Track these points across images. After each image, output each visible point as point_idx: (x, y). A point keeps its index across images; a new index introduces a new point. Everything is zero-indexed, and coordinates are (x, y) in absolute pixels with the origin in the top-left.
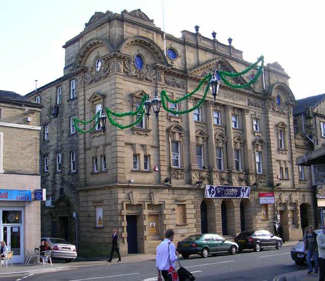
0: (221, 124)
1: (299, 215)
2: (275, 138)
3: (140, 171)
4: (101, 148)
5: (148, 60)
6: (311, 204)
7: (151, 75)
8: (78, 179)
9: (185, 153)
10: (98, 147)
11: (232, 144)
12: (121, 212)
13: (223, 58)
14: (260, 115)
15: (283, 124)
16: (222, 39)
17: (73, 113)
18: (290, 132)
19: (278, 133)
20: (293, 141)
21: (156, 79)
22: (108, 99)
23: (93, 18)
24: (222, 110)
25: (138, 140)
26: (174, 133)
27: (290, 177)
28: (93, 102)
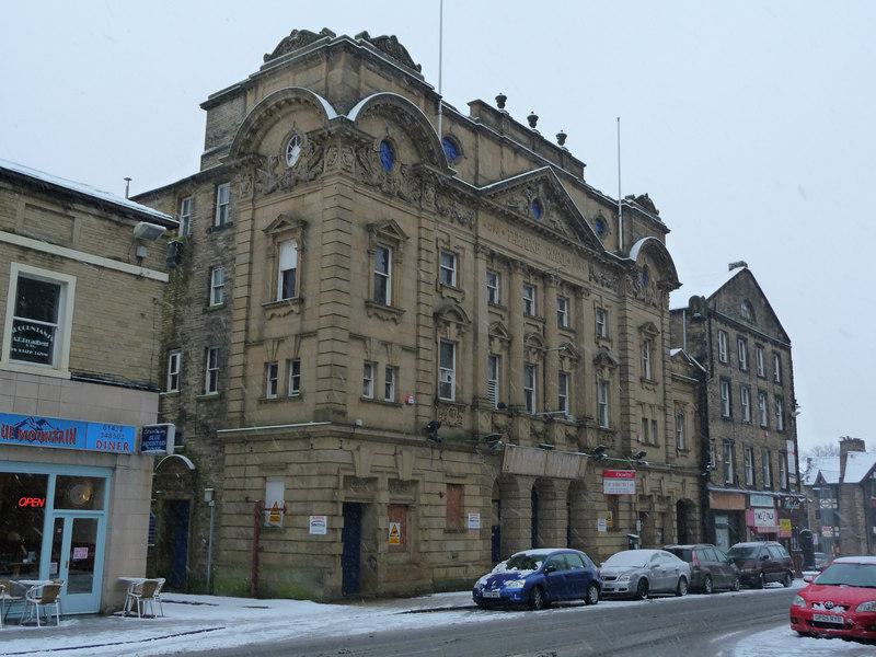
3: (375, 402)
4: (291, 343)
5: (406, 155)
6: (696, 502)
8: (222, 412)
9: (469, 370)
10: (280, 341)
13: (551, 169)
16: (548, 132)
17: (218, 258)
22: (314, 232)
23: (285, 45)
24: (539, 284)
26: (447, 323)
27: (661, 441)
28: (275, 236)
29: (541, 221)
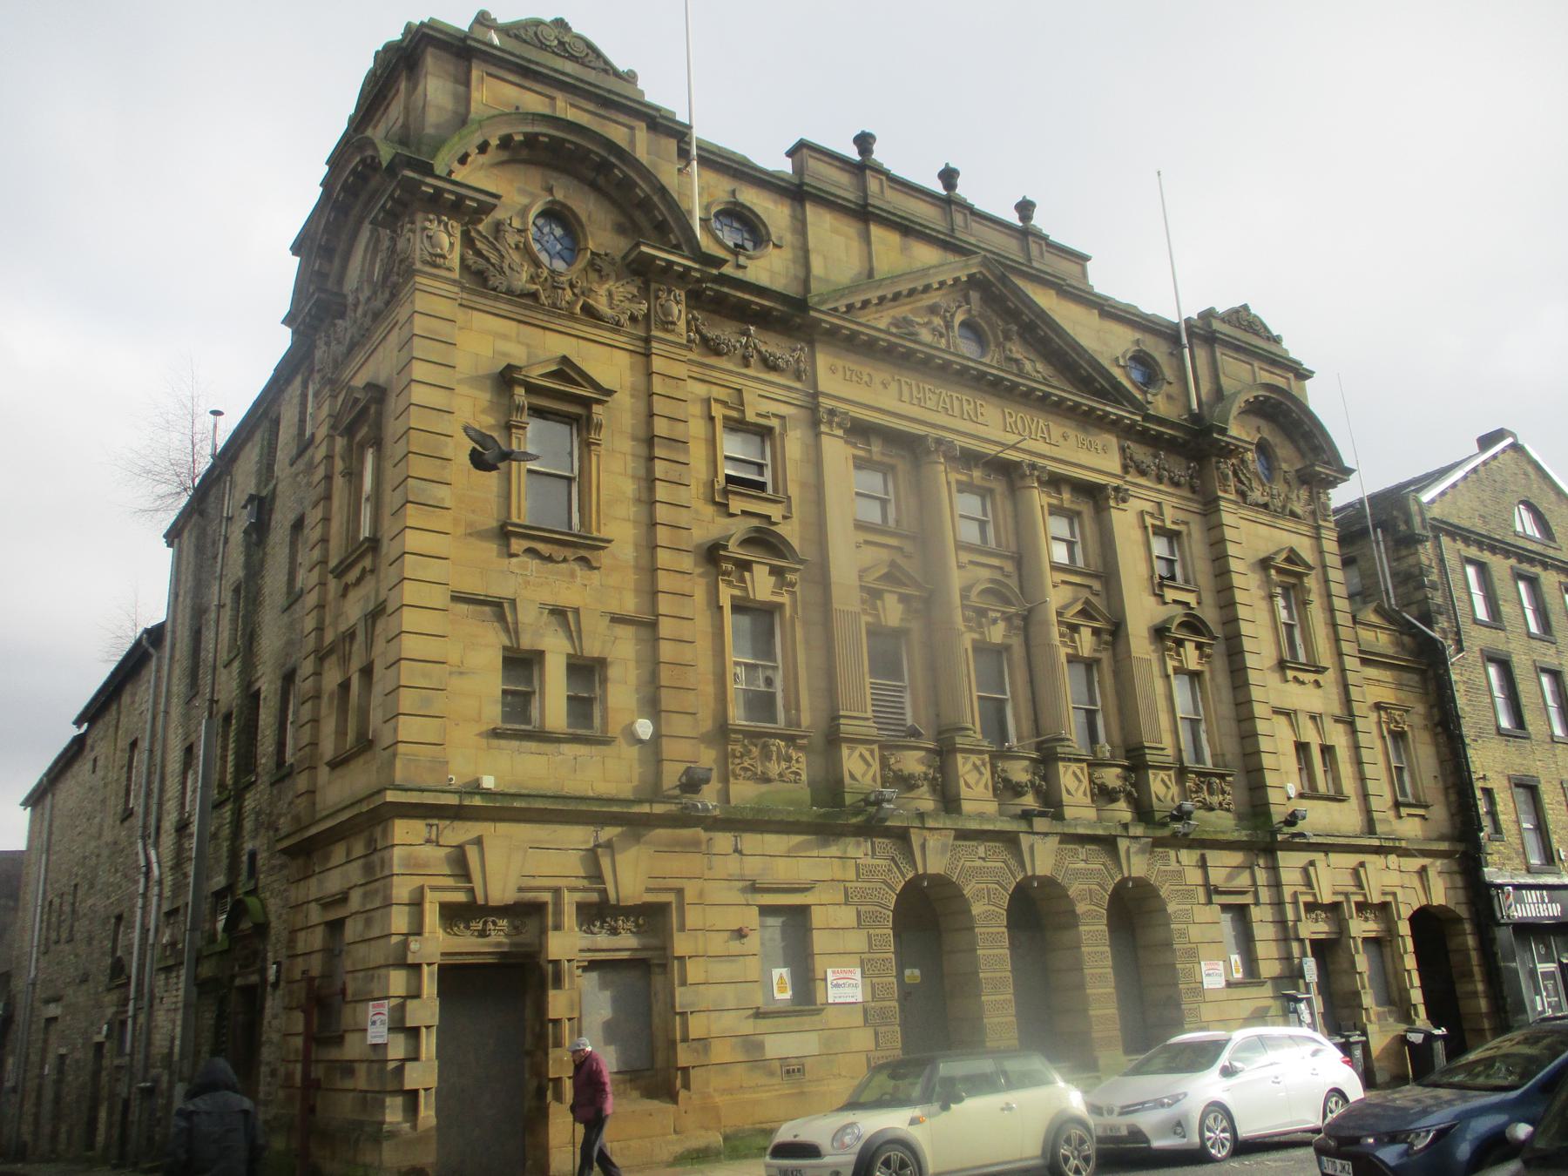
0: (999, 544)
1: (1410, 962)
2: (1263, 617)
6: (1463, 911)
7: (611, 295)
11: (1048, 633)
12: (405, 945)
14: (1181, 516)
15: (1293, 557)
16: (989, 193)
18: (1329, 595)
19: (1271, 597)
20: (1344, 633)
21: (647, 316)
25: (533, 586)
27: (1349, 786)
29: (986, 360)
